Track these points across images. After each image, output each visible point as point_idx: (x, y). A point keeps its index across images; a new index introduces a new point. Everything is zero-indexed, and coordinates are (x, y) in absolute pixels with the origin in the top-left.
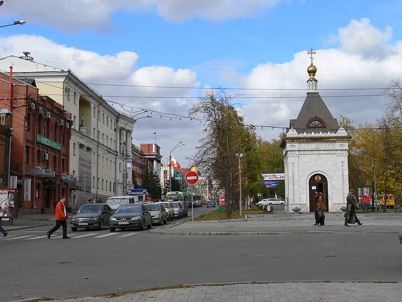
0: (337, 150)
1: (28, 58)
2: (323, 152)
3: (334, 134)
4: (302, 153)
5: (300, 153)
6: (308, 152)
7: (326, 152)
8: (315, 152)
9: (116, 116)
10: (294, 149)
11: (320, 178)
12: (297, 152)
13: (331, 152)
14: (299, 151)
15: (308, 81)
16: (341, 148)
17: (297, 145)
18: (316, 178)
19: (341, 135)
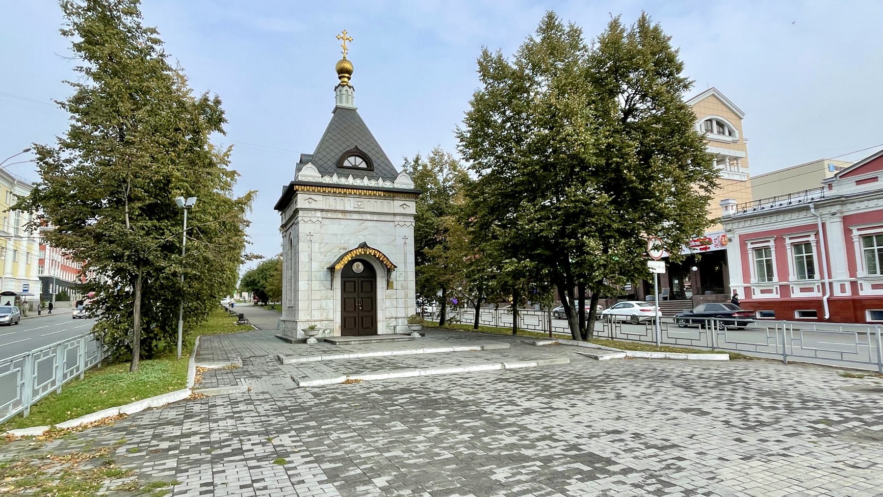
0: (395, 214)
2: (369, 217)
8: (355, 216)
12: (319, 214)
16: (403, 211)
17: (319, 198)
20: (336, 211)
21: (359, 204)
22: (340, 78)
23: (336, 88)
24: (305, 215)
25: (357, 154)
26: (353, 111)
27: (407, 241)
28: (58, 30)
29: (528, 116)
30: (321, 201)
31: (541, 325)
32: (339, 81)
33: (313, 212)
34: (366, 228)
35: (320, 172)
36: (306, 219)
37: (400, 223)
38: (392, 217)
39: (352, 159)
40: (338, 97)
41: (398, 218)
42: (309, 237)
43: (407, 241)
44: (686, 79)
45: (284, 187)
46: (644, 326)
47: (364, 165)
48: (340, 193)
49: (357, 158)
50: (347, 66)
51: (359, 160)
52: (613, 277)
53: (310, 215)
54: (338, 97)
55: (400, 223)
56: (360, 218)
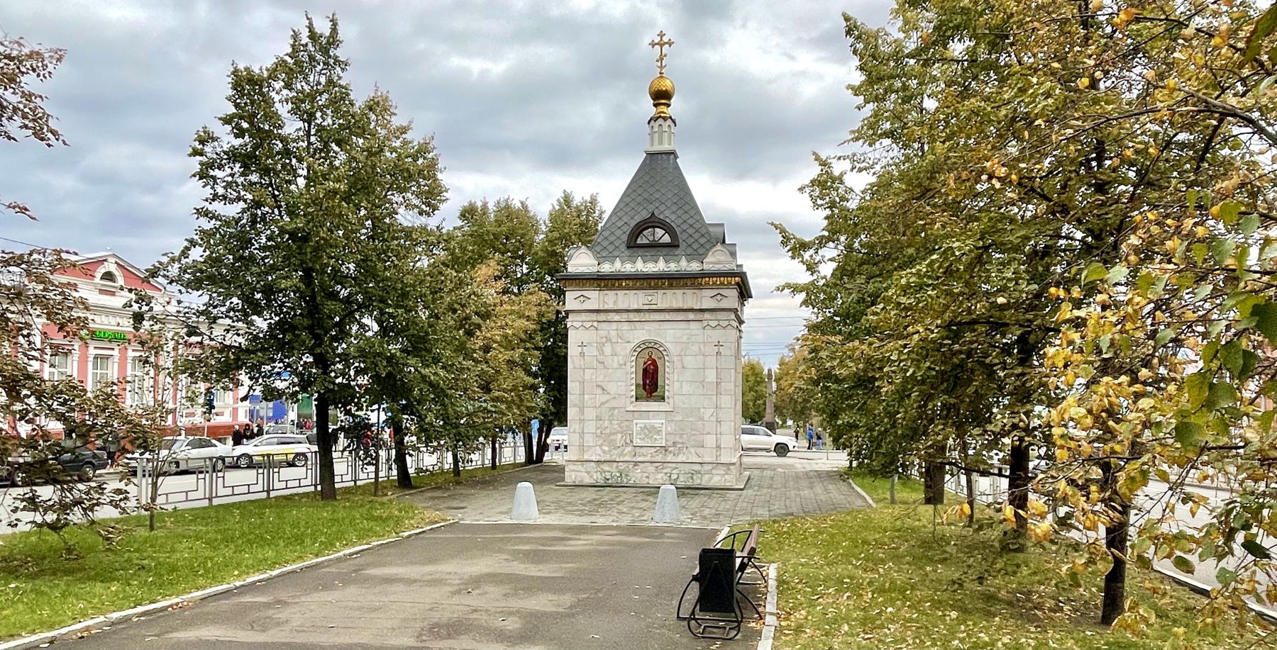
20: (628, 311)
21: (650, 298)
22: (655, 105)
23: (649, 123)
28: (843, 87)
29: (947, 123)
30: (595, 298)
31: (260, 482)
32: (653, 111)
36: (577, 324)
37: (710, 323)
40: (656, 136)
41: (707, 315)
44: (295, 36)
46: (195, 476)
47: (667, 239)
50: (666, 85)
51: (659, 232)
54: (656, 136)
55: (710, 323)
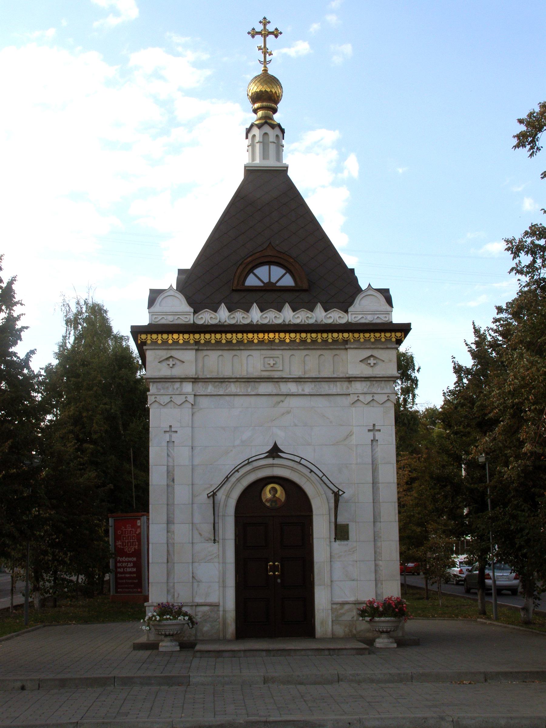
0: (350, 379)
1: (68, 335)
2: (293, 388)
3: (342, 314)
4: (210, 389)
5: (201, 388)
6: (233, 388)
7: (308, 388)
8: (264, 388)
9: (334, 492)
10: (178, 371)
11: (280, 493)
12: (188, 387)
13: (326, 388)
14: (195, 380)
15: (248, 131)
16: (367, 371)
17: (189, 355)
18: (267, 494)
19: (369, 319)
24: (162, 392)
25: (250, 266)
26: (131, 332)
27: (378, 435)
33: (177, 385)
34: (288, 412)
35: (191, 303)
38: (346, 384)
39: (262, 272)
41: (358, 387)
42: (167, 435)
43: (378, 435)
45: (181, 272)
48: (293, 342)
49: (256, 271)
51: (277, 272)
52: (480, 399)
53: (170, 391)
56: (275, 392)
